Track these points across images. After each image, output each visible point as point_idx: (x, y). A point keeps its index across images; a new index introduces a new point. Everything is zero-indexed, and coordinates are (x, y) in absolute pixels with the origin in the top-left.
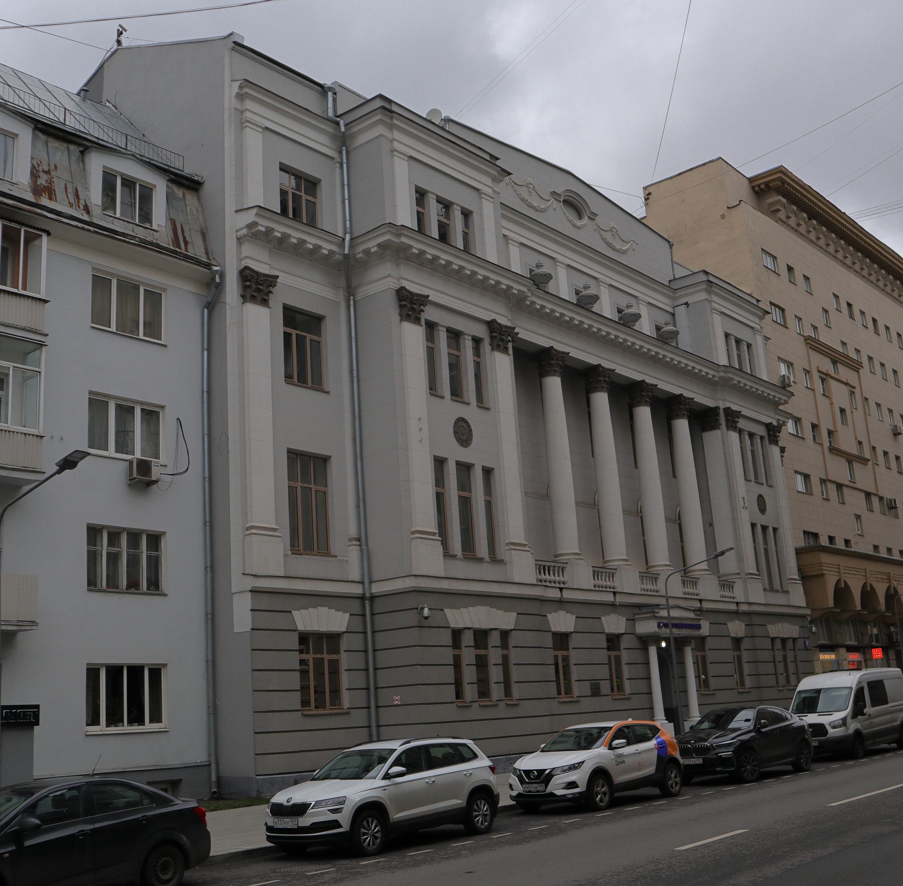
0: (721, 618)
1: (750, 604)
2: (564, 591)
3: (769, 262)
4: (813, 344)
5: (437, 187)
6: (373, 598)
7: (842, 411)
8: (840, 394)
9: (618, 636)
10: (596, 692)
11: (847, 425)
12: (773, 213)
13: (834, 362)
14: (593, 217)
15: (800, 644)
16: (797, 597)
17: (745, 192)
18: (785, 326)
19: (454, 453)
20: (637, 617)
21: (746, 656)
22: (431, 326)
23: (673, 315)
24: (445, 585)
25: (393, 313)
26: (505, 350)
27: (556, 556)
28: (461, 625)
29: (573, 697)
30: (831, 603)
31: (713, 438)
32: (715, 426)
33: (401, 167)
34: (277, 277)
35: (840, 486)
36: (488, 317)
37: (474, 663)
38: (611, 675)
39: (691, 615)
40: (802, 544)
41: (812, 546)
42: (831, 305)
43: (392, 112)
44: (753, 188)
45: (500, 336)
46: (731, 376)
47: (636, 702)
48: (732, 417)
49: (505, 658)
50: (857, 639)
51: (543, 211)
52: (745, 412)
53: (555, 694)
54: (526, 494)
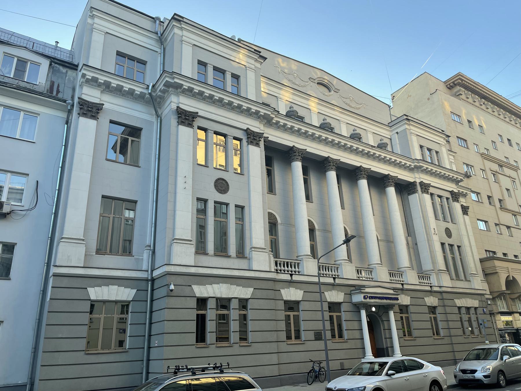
0: (419, 295)
1: (440, 287)
2: (293, 276)
3: (456, 119)
4: (486, 157)
5: (427, 144)
6: (153, 280)
7: (508, 190)
8: (506, 182)
9: (435, 308)
10: (318, 336)
11: (511, 197)
12: (458, 95)
13: (501, 166)
14: (337, 91)
15: (480, 311)
16: (479, 284)
17: (442, 88)
18: (468, 148)
19: (213, 196)
20: (352, 292)
21: (439, 317)
22: (432, 194)
23: (391, 139)
24: (193, 270)
25: (174, 121)
26: (257, 145)
27: (398, 269)
28: (205, 295)
29: (301, 341)
30: (504, 288)
31: (414, 199)
32: (414, 191)
33: (414, 138)
34: (103, 105)
35: (508, 227)
36: (451, 190)
37: (238, 319)
38: (432, 326)
39: (391, 292)
40: (484, 255)
41: (489, 258)
42: (498, 140)
43: (409, 120)
44: (447, 86)
45: (253, 138)
46: (421, 164)
47: (351, 344)
48: (425, 187)
49: (244, 318)
50: (508, 308)
51: (359, 109)
52: (432, 184)
53: (462, 334)
54: (294, 226)
